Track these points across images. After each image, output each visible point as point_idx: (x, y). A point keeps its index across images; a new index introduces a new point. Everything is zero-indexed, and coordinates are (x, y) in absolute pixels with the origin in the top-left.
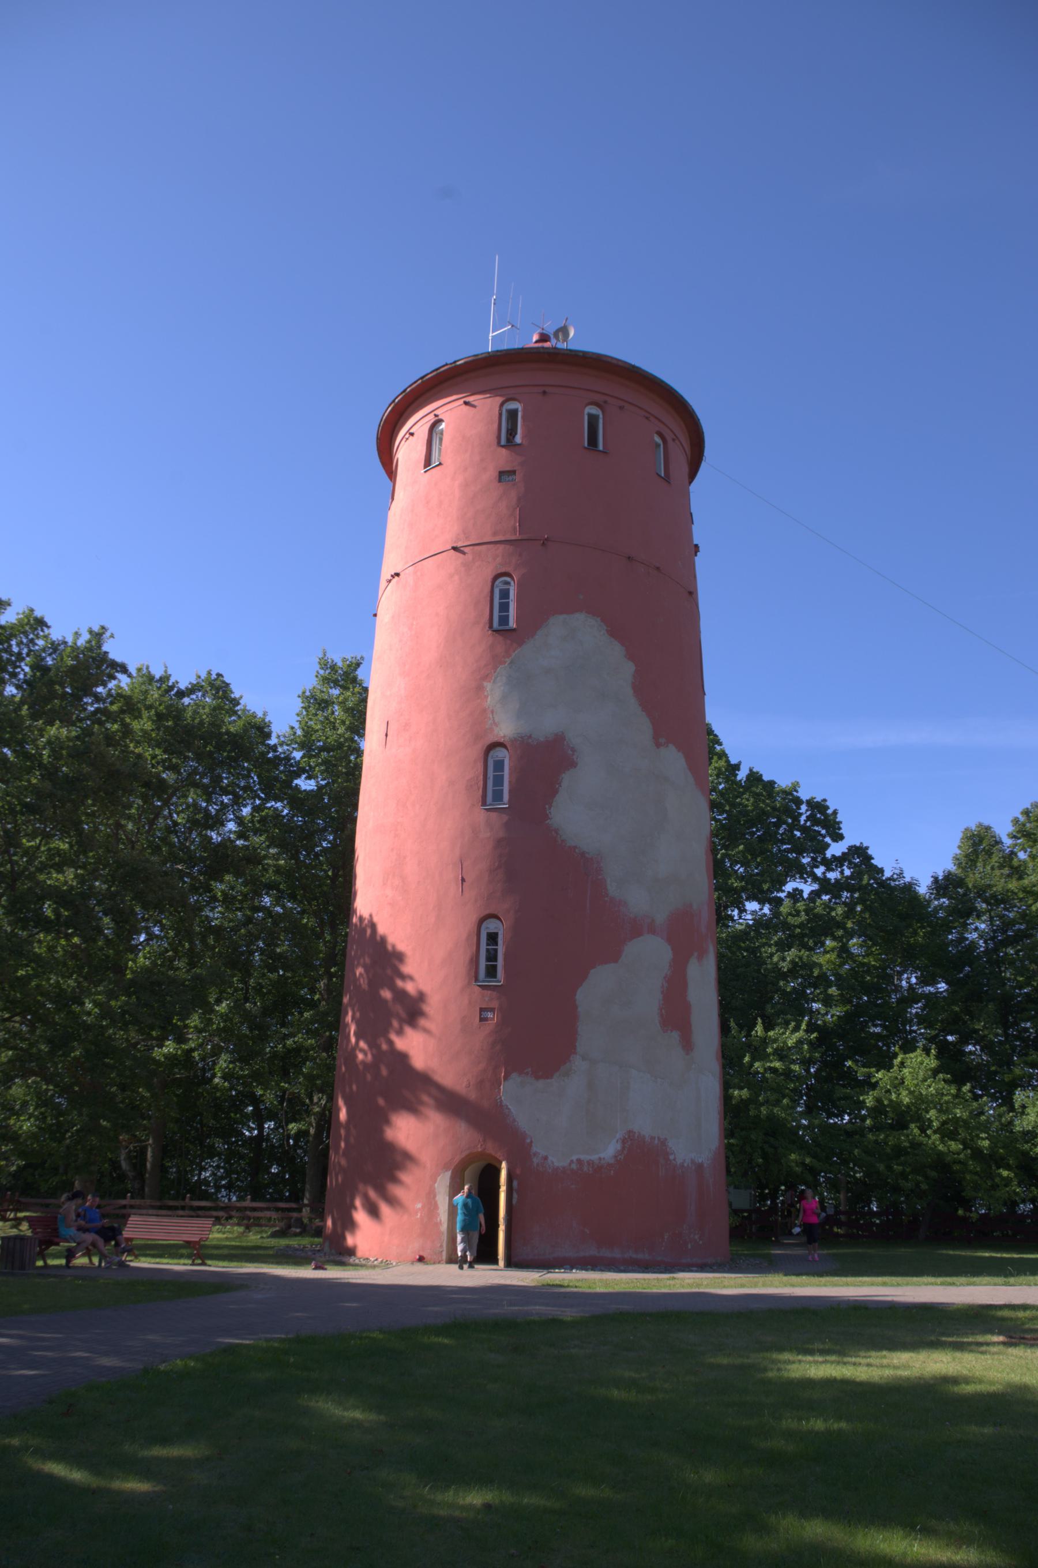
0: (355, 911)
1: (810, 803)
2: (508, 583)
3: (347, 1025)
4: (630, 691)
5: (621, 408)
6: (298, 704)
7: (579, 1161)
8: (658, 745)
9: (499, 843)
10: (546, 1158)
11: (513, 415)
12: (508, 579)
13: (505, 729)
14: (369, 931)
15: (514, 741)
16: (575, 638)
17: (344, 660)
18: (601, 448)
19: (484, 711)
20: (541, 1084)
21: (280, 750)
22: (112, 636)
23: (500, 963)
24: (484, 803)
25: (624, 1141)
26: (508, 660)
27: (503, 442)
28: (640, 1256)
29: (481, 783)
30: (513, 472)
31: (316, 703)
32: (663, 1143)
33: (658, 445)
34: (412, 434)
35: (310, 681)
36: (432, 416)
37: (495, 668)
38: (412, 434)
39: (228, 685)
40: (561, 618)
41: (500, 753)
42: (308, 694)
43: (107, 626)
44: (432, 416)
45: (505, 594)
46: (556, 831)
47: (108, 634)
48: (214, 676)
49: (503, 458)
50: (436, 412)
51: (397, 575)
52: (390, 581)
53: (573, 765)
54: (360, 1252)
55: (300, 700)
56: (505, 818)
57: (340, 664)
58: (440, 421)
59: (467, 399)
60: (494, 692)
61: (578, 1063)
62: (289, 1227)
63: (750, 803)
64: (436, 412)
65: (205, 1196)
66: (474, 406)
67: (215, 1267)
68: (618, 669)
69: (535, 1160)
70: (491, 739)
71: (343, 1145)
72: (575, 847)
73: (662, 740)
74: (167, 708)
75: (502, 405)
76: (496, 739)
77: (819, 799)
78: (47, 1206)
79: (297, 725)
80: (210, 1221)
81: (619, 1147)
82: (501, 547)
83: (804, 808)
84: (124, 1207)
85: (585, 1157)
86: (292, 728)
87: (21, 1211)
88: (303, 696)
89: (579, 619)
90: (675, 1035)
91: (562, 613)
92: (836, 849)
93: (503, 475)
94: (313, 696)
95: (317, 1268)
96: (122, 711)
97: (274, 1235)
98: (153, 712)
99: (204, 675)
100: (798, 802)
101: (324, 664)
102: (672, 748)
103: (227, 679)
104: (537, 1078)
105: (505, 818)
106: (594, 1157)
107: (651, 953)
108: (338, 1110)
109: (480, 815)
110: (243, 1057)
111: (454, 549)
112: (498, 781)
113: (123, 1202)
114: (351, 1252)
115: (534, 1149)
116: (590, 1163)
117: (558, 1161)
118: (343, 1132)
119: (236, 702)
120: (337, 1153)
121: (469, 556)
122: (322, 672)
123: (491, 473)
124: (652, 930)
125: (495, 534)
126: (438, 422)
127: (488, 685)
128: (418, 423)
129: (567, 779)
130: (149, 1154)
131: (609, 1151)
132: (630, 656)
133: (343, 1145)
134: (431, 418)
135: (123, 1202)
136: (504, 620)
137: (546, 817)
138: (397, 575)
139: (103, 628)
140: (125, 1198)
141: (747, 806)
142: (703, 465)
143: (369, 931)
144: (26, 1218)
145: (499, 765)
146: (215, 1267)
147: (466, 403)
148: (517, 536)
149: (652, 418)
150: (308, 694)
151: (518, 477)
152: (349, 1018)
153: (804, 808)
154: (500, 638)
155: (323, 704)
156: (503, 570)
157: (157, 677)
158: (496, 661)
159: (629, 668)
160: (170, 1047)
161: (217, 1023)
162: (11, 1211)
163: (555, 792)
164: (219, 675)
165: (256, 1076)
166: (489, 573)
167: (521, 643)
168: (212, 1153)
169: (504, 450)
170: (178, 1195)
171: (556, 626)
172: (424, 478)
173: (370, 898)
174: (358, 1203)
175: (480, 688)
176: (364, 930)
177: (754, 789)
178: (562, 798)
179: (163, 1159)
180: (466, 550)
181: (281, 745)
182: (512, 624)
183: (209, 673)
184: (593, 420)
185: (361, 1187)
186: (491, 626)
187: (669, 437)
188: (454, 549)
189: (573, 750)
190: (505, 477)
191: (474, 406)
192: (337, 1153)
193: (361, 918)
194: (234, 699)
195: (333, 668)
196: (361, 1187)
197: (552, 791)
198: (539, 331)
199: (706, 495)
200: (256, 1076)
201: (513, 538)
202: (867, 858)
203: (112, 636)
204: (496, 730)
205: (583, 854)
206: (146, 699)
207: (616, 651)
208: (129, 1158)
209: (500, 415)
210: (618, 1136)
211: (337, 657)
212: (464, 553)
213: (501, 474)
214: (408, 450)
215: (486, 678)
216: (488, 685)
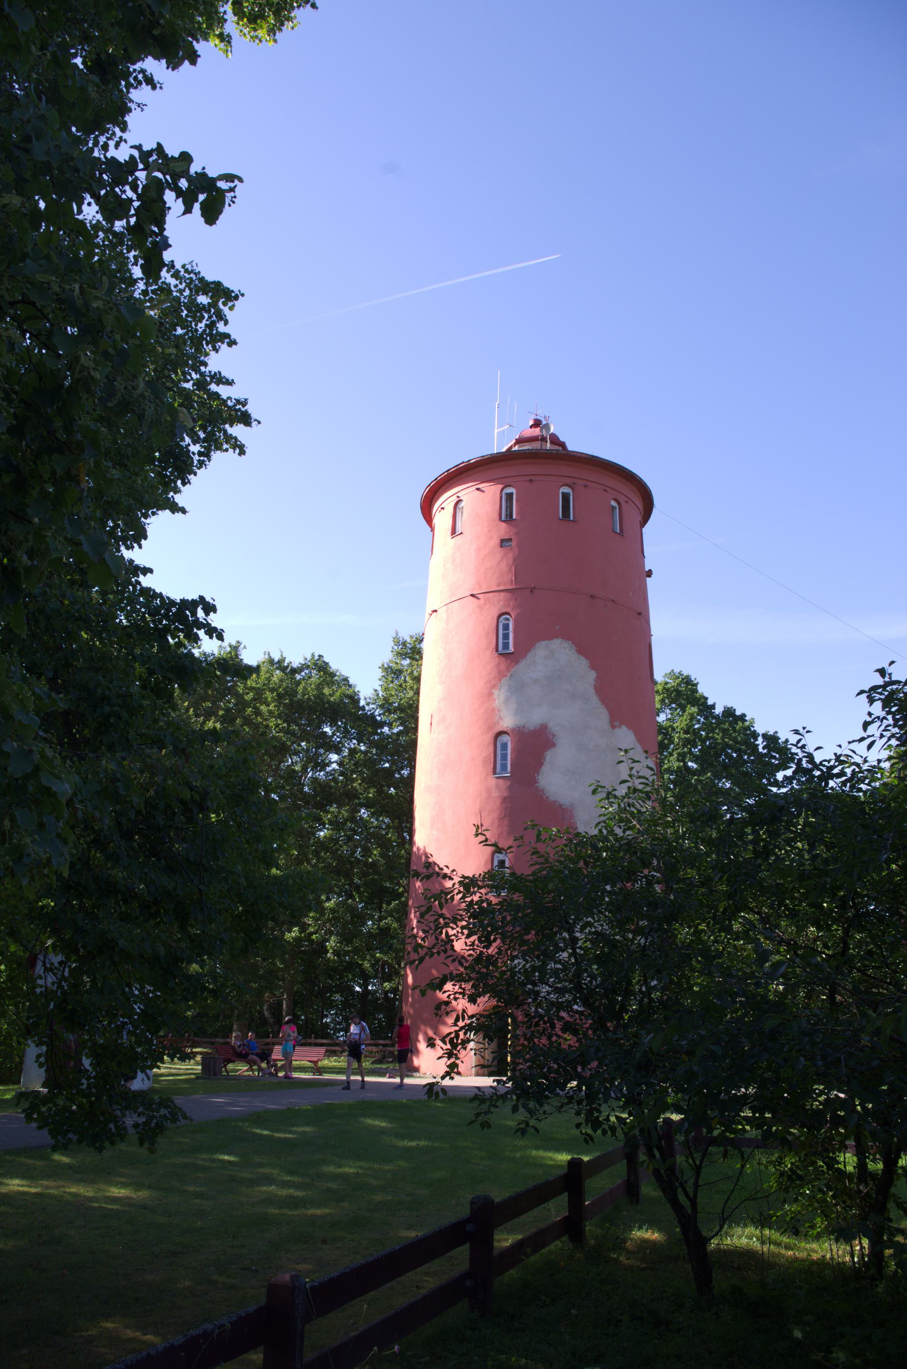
0: (415, 843)
1: (765, 736)
2: (508, 619)
3: (411, 920)
4: (592, 691)
5: (586, 486)
6: (380, 673)
9: (504, 800)
11: (510, 496)
12: (508, 617)
13: (508, 722)
14: (423, 858)
15: (513, 730)
16: (555, 656)
17: (411, 637)
18: (572, 518)
19: (493, 709)
21: (367, 708)
22: (245, 647)
24: (495, 773)
26: (509, 674)
27: (503, 518)
29: (492, 760)
30: (510, 540)
31: (392, 672)
33: (613, 508)
34: (443, 508)
35: (386, 655)
36: (455, 497)
37: (500, 680)
38: (443, 508)
39: (327, 664)
40: (544, 643)
41: (505, 738)
42: (386, 666)
43: (241, 640)
44: (455, 497)
45: (506, 627)
46: (543, 791)
47: (242, 646)
48: (316, 657)
49: (503, 529)
51: (436, 611)
53: (553, 745)
54: (422, 1070)
55: (380, 670)
56: (508, 783)
57: (409, 640)
58: (461, 500)
59: (478, 486)
60: (500, 696)
62: (384, 1057)
63: (719, 737)
65: (327, 1036)
66: (483, 491)
67: (327, 1076)
68: (584, 676)
70: (498, 729)
71: (410, 999)
72: (555, 802)
73: (616, 723)
74: (284, 689)
75: (502, 490)
76: (501, 729)
77: (771, 733)
78: (213, 1043)
79: (379, 688)
80: (323, 1050)
82: (503, 594)
83: (760, 740)
84: (268, 1044)
86: (376, 691)
87: (196, 1047)
88: (382, 667)
91: (544, 639)
93: (503, 542)
94: (390, 667)
95: (390, 1077)
96: (254, 699)
97: (373, 1063)
98: (275, 694)
99: (309, 657)
100: (755, 735)
101: (397, 641)
102: (624, 728)
103: (326, 659)
105: (508, 783)
108: (407, 976)
109: (492, 781)
110: (346, 938)
111: (472, 595)
112: (504, 757)
113: (268, 1040)
114: (417, 1070)
118: (410, 991)
119: (333, 675)
120: (406, 1005)
121: (482, 601)
122: (396, 647)
123: (495, 541)
125: (499, 585)
126: (459, 501)
127: (496, 692)
128: (446, 500)
129: (549, 755)
130: (284, 1006)
132: (593, 667)
133: (410, 999)
134: (455, 499)
135: (268, 1040)
136: (506, 646)
137: (536, 782)
138: (436, 611)
139: (238, 642)
140: (268, 1037)
141: (717, 739)
142: (654, 511)
143: (423, 858)
144: (200, 1053)
145: (504, 746)
146: (327, 1076)
147: (478, 489)
148: (514, 587)
149: (608, 490)
150: (386, 666)
151: (514, 544)
152: (412, 915)
153: (760, 740)
154: (504, 659)
155: (397, 673)
156: (504, 611)
157: (276, 660)
158: (501, 675)
159: (593, 675)
160: (295, 932)
161: (328, 915)
162: (189, 1047)
163: (541, 764)
164: (320, 656)
165: (356, 951)
166: (495, 613)
167: (517, 662)
168: (330, 1005)
169: (504, 524)
170: (313, 1034)
171: (541, 650)
172: (452, 542)
173: (424, 837)
174: (421, 1037)
175: (490, 694)
176: (420, 857)
177: (722, 726)
178: (545, 769)
179: (294, 1009)
180: (479, 596)
181: (368, 704)
182: (511, 649)
183: (313, 655)
184: (566, 497)
185: (422, 1027)
186: (497, 650)
187: (622, 499)
188: (472, 595)
189: (553, 735)
190: (504, 544)
191: (483, 491)
192: (406, 1005)
193: (418, 849)
194: (332, 673)
195: (404, 644)
196: (422, 1027)
197: (539, 763)
198: (534, 417)
199: (653, 534)
200: (356, 951)
201: (511, 587)
203: (245, 647)
204: (501, 723)
205: (560, 806)
206: (269, 683)
207: (582, 664)
208: (271, 1008)
209: (501, 497)
211: (406, 635)
212: (478, 599)
213: (502, 541)
214: (442, 518)
215: (494, 687)
216: (496, 692)
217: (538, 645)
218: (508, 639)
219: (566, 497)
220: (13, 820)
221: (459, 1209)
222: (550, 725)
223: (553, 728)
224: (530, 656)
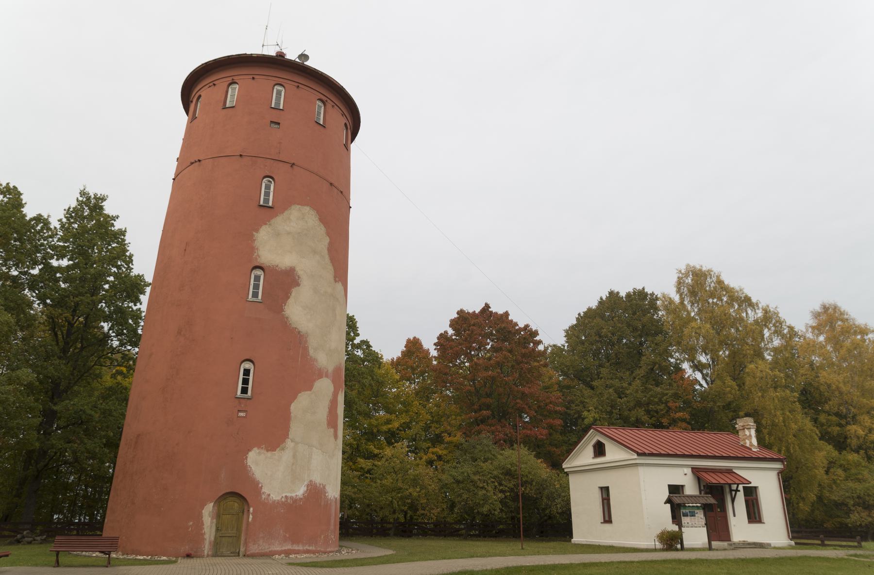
4: (326, 252)
7: (286, 497)
8: (336, 281)
10: (269, 495)
20: (269, 454)
23: (250, 386)
25: (308, 486)
28: (311, 548)
32: (324, 487)
40: (298, 207)
46: (287, 318)
50: (235, 78)
52: (192, 163)
53: (298, 285)
61: (289, 443)
64: (235, 78)
69: (263, 496)
81: (305, 489)
85: (289, 495)
89: (307, 209)
90: (332, 430)
92: (357, 341)
104: (268, 451)
106: (294, 495)
107: (325, 387)
115: (263, 490)
116: (291, 498)
117: (275, 496)
124: (327, 376)
129: (294, 291)
131: (300, 491)
137: (282, 310)
138: (199, 161)
159: (327, 240)
163: (289, 298)
178: (291, 301)
183: (8, 184)
184: (247, 372)
202: (369, 346)
205: (299, 332)
210: (306, 483)
217: (293, 207)
218: (269, 196)
219: (247, 372)
220: (747, 314)
221: (292, 162)
222: (297, 269)
223: (300, 271)
224: (286, 213)
